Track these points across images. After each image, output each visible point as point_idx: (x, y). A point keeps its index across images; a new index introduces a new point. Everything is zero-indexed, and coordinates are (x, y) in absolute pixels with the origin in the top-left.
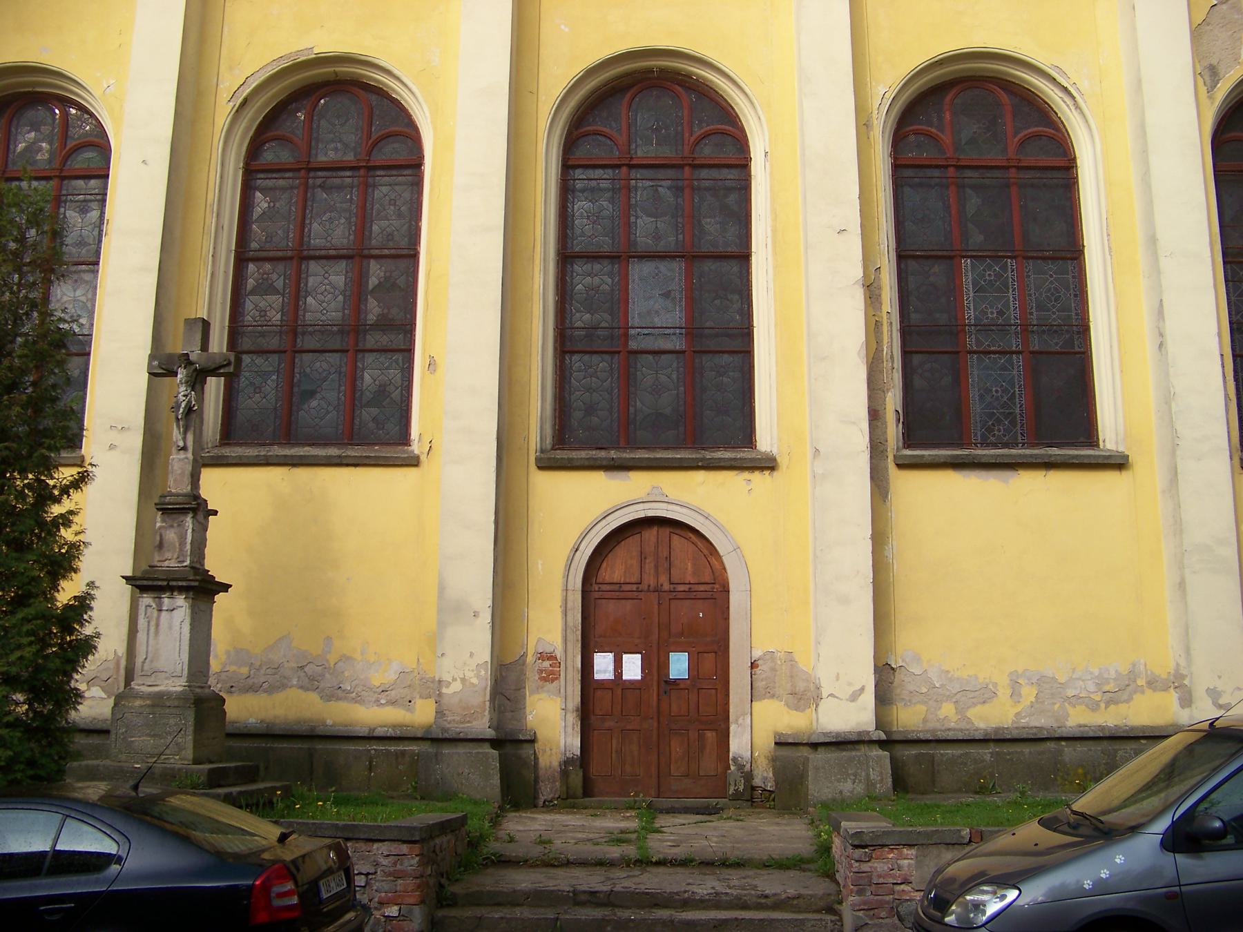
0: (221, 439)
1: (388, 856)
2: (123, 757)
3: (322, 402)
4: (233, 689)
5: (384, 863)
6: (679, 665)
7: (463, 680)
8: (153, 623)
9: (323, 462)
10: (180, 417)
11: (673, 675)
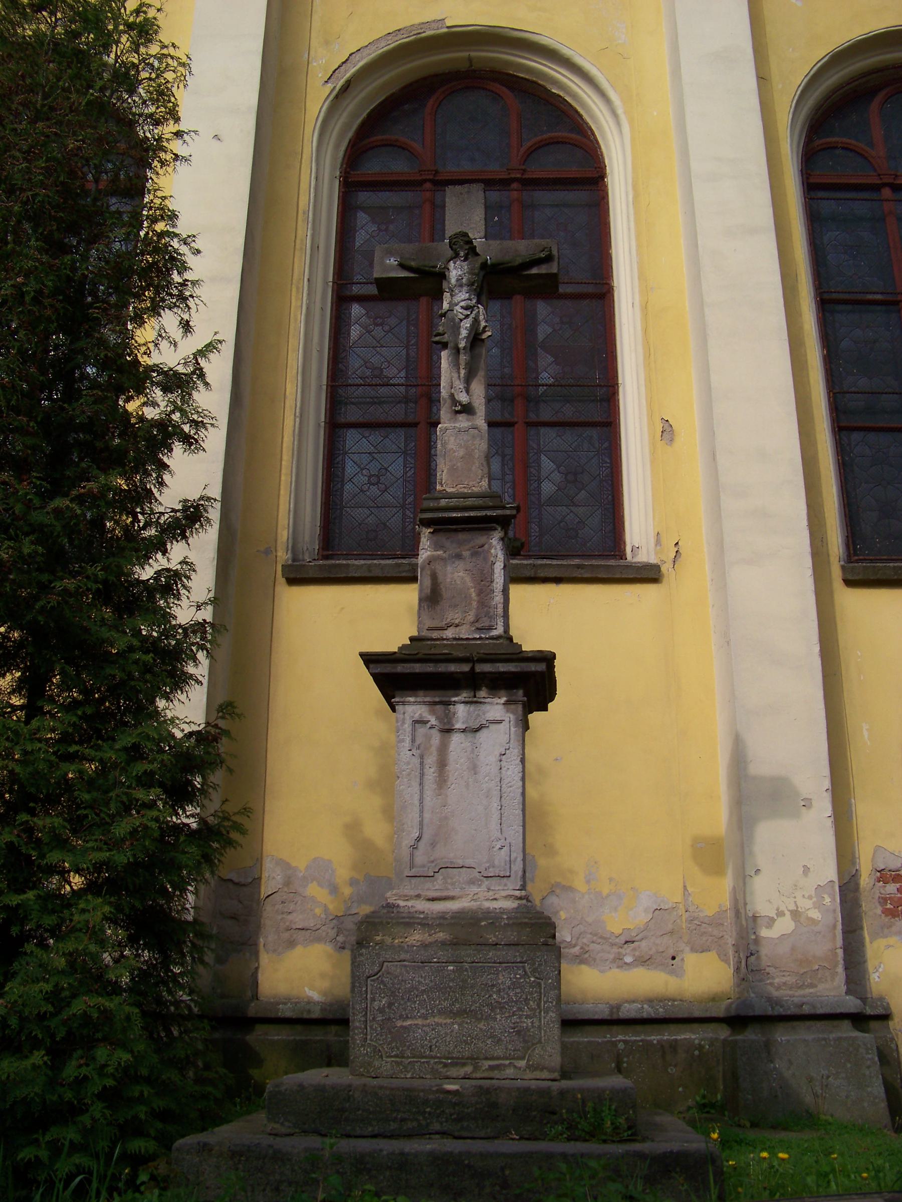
2: (385, 1066)
7: (796, 914)
8: (431, 760)
10: (462, 344)
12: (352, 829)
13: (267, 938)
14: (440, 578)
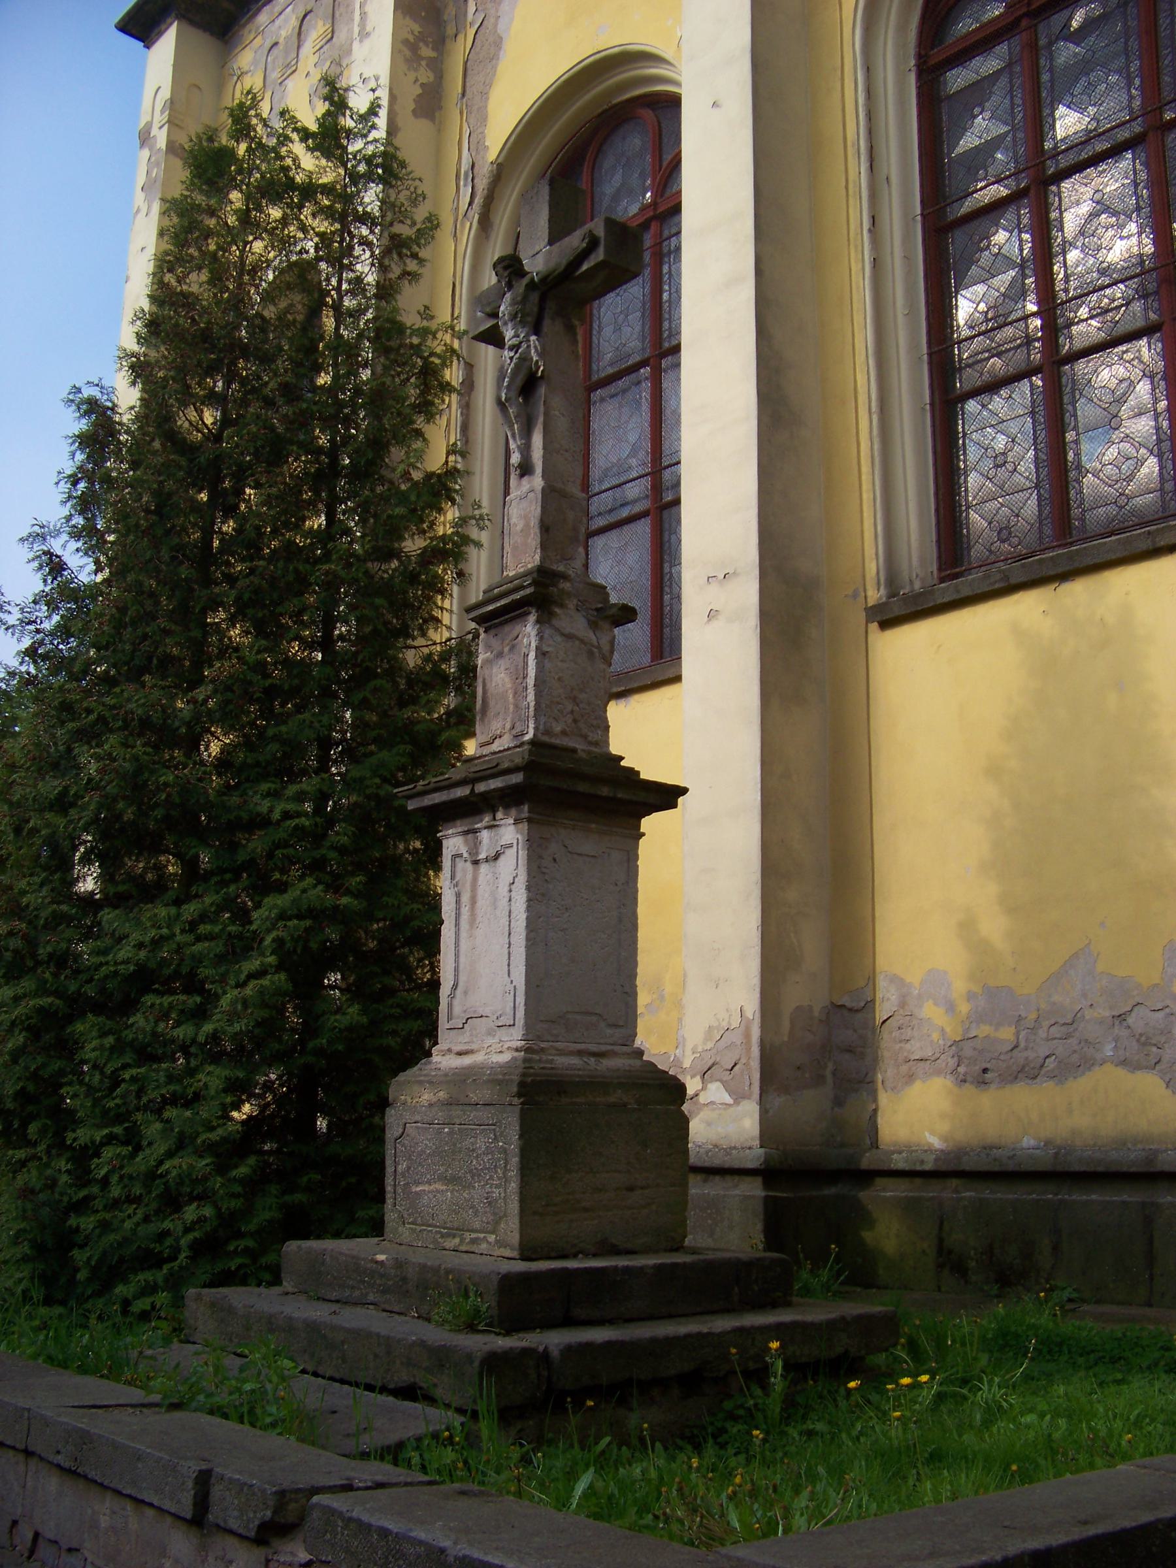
0: (940, 569)
3: (1125, 446)
4: (988, 1076)
9: (1119, 555)
12: (967, 928)
13: (886, 1073)
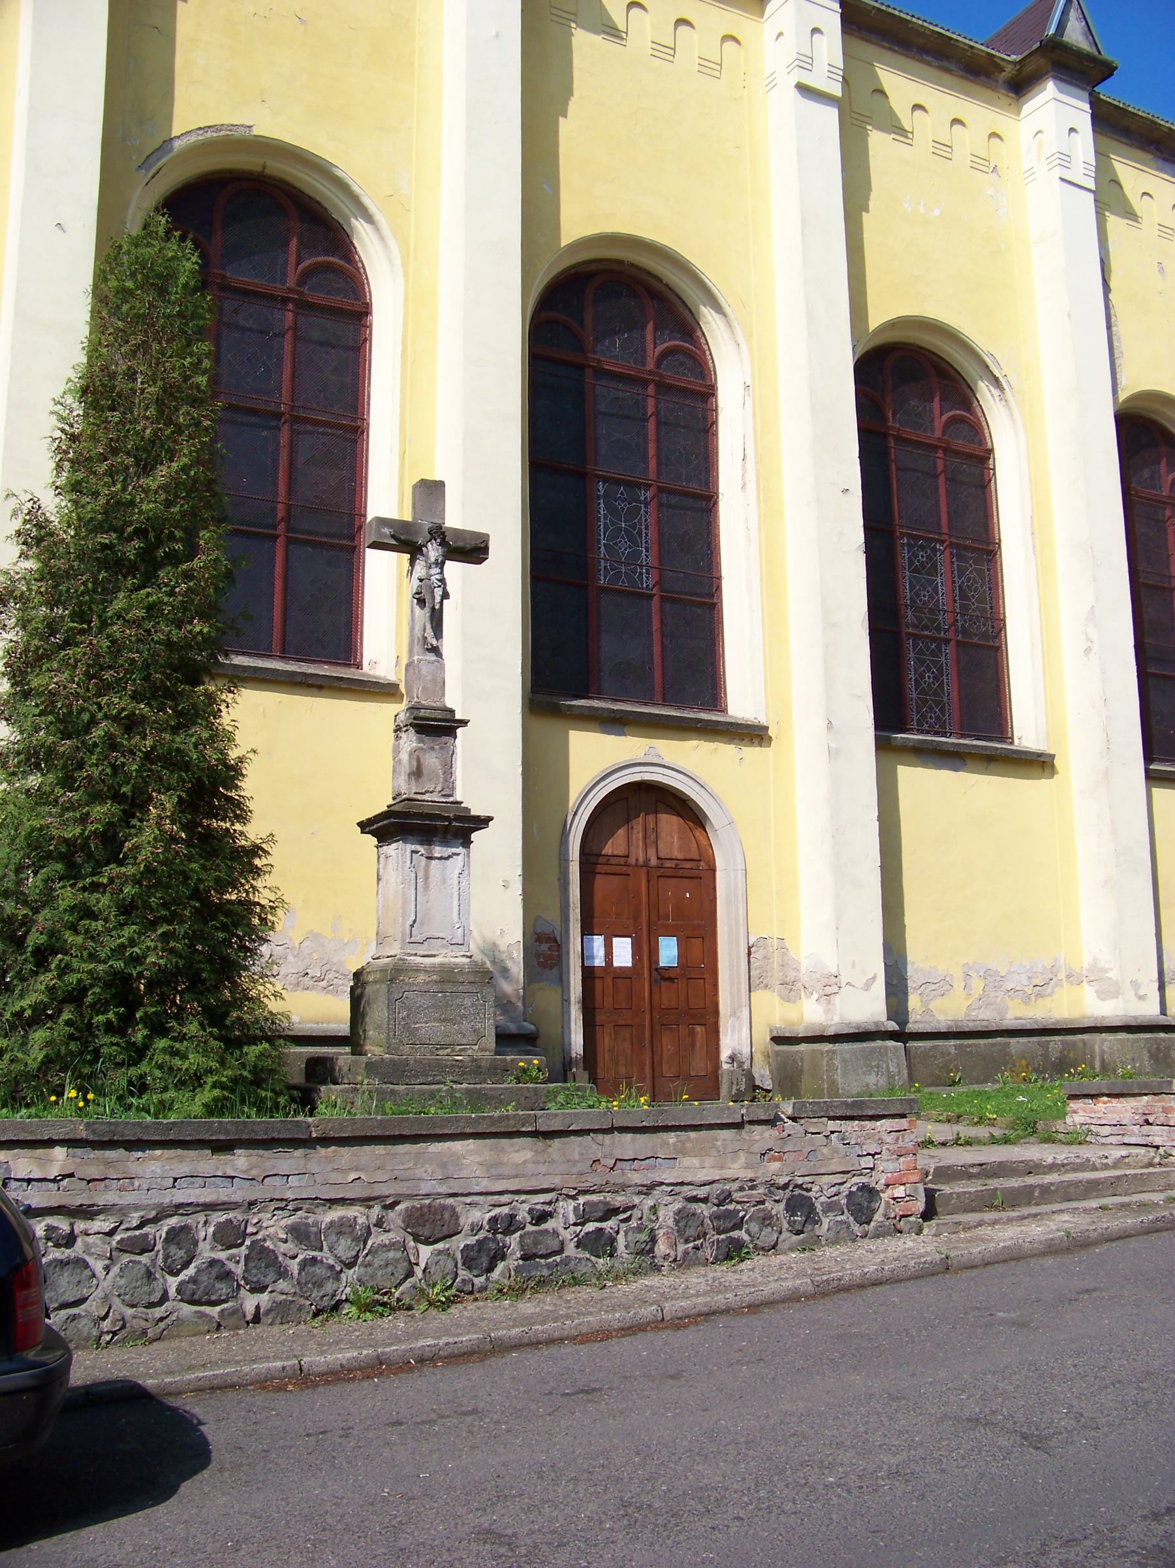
1: (891, 1132)
5: (888, 1141)
6: (668, 951)
11: (663, 963)
14: (422, 760)
